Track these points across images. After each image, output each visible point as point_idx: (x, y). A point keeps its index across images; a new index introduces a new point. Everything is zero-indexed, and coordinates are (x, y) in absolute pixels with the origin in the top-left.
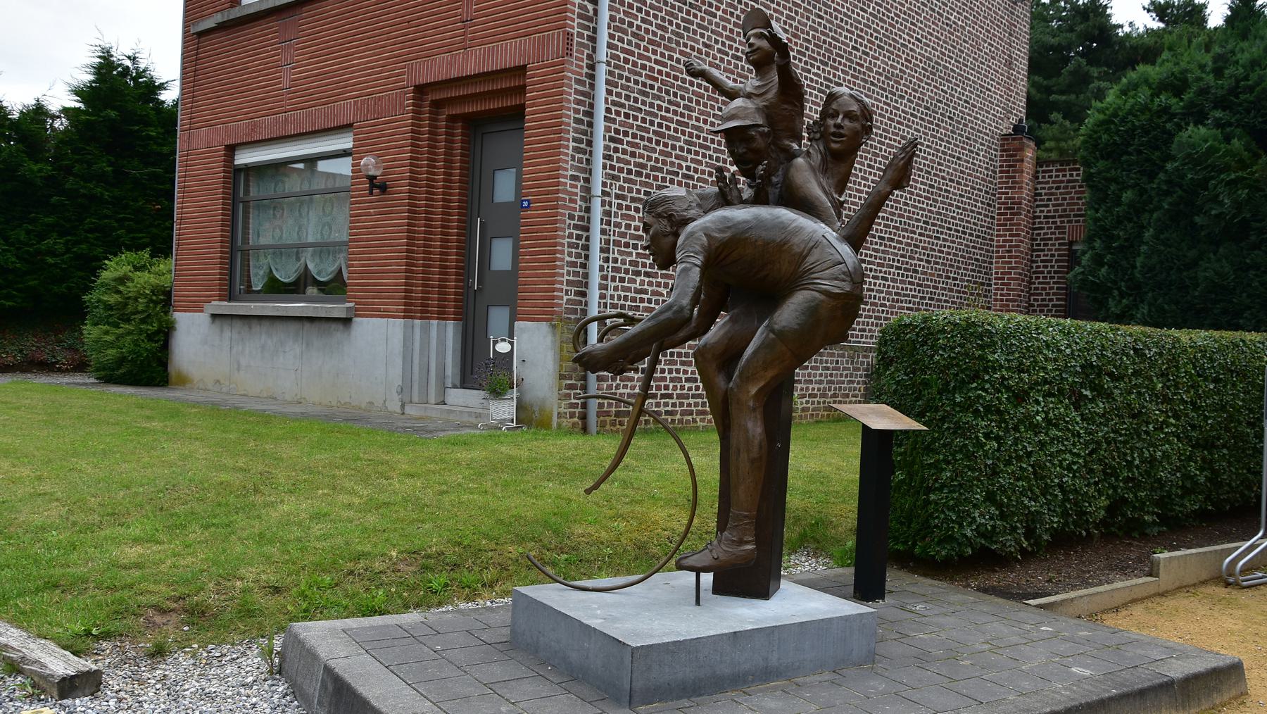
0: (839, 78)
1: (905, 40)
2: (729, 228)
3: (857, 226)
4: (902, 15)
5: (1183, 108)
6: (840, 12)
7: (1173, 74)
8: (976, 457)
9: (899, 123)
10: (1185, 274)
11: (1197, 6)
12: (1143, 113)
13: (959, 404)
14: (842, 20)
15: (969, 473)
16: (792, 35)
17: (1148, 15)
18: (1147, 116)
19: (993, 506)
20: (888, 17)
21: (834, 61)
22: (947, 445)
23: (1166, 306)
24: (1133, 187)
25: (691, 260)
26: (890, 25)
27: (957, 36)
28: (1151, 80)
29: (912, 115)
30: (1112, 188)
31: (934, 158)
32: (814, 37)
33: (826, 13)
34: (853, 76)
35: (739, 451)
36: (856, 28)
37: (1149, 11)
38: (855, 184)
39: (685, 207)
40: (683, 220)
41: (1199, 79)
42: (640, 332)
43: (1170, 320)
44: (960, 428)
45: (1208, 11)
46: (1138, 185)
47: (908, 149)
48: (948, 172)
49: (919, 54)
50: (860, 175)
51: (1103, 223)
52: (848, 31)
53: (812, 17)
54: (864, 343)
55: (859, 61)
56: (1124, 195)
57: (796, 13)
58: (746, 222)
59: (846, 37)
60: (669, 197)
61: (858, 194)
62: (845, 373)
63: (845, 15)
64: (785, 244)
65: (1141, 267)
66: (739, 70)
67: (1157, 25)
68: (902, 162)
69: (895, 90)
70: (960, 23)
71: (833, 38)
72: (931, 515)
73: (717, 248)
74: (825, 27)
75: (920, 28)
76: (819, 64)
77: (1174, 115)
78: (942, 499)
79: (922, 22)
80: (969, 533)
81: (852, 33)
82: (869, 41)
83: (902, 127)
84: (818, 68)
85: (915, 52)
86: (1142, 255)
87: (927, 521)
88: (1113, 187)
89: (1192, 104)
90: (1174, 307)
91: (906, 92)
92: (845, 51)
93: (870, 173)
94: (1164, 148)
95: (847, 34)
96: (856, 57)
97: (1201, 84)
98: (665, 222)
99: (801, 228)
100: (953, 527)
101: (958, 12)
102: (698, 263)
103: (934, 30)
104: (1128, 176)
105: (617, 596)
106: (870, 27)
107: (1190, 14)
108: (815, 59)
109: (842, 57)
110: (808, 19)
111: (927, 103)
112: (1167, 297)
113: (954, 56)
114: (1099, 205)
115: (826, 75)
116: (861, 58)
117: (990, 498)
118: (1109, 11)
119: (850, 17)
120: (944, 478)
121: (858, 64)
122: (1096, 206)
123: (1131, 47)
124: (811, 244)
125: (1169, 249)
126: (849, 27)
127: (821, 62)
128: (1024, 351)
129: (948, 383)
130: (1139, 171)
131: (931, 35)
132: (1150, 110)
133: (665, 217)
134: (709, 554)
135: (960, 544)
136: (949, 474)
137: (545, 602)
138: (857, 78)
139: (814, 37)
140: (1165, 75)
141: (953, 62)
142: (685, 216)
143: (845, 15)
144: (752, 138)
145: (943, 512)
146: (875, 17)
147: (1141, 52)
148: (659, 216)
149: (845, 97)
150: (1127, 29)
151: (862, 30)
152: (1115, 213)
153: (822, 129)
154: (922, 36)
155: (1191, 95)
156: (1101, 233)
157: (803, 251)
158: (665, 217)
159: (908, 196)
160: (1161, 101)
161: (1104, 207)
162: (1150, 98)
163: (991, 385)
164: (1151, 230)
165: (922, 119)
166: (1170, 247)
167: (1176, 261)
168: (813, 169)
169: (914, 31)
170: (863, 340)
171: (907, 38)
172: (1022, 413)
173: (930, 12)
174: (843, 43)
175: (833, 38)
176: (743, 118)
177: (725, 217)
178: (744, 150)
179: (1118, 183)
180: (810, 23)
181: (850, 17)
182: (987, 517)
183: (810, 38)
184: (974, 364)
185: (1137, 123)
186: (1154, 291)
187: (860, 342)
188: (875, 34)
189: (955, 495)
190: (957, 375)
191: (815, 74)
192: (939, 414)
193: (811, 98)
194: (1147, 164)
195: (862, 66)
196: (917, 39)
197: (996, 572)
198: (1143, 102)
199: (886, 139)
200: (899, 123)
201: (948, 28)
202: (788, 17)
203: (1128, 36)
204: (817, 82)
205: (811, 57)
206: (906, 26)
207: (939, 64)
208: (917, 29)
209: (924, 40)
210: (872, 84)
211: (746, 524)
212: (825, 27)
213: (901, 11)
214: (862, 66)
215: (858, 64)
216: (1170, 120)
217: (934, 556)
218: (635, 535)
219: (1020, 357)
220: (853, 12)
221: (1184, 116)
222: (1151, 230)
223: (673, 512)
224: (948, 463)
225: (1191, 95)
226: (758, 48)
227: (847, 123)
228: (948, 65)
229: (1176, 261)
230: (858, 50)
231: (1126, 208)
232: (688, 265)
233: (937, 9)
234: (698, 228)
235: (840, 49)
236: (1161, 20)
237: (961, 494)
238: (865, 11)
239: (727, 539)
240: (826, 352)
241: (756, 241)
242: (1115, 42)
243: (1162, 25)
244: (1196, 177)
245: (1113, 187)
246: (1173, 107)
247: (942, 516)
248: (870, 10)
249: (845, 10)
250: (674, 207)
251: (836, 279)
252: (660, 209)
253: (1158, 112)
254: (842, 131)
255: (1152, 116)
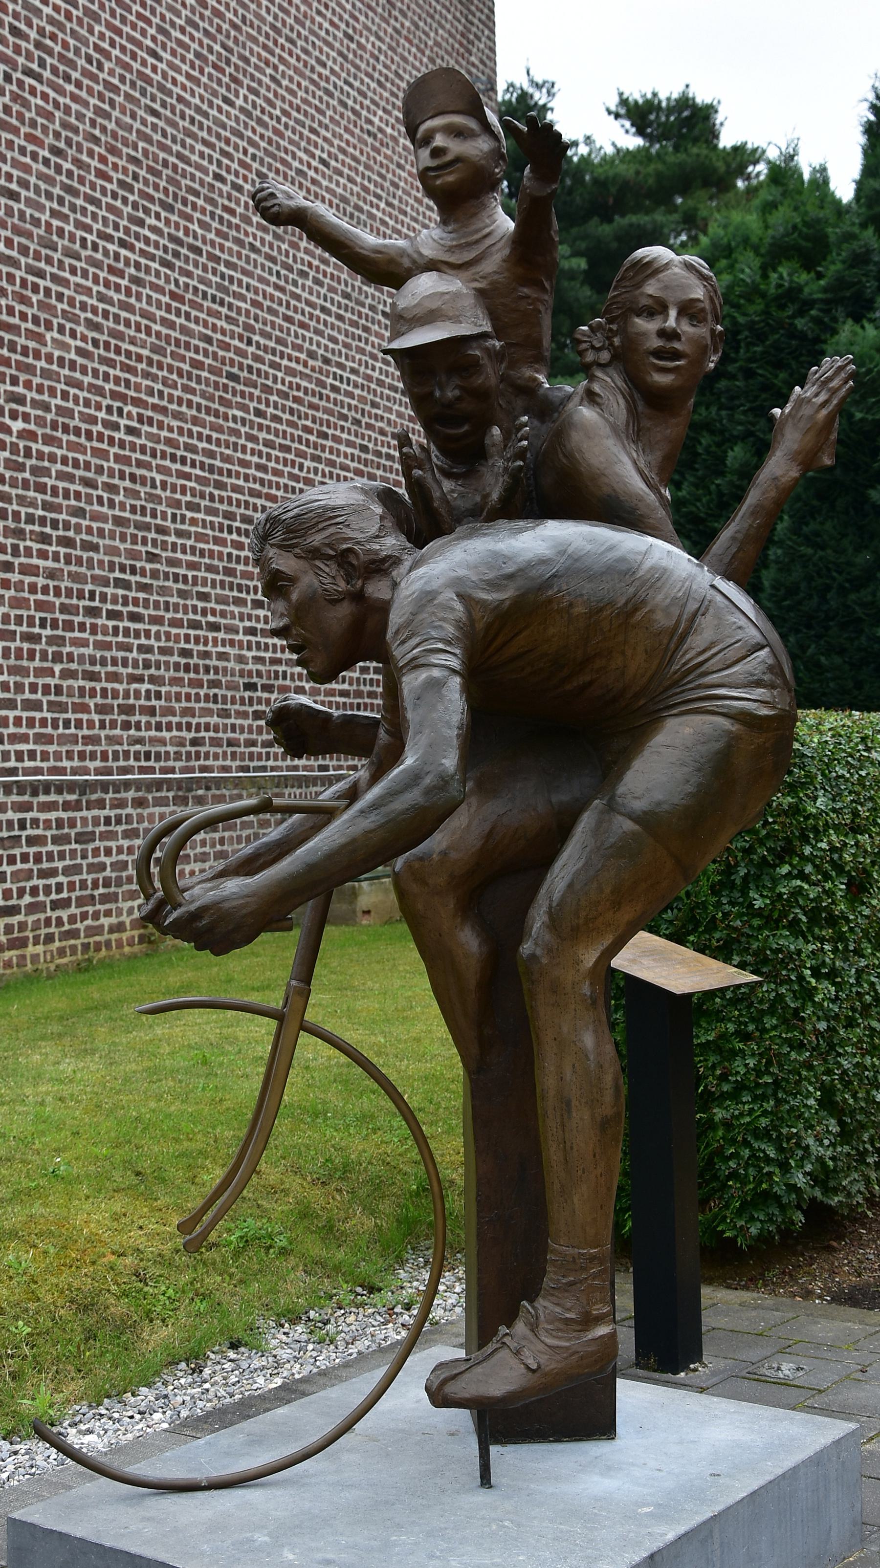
0: (195, 237)
1: (301, 161)
2: (511, 577)
3: (734, 557)
4: (294, 114)
5: (825, 290)
6: (188, 104)
7: (795, 227)
8: (803, 1019)
9: (303, 325)
10: (853, 597)
11: (701, 109)
12: (750, 301)
13: (759, 913)
14: (192, 121)
15: (793, 1055)
16: (107, 150)
17: (617, 124)
18: (759, 306)
19: (832, 1116)
20: (271, 116)
21: (185, 202)
22: (741, 1000)
23: (823, 659)
24: (744, 437)
25: (436, 659)
26: (276, 131)
27: (386, 157)
28: (754, 239)
29: (323, 309)
30: (703, 441)
31: (365, 394)
32: (146, 152)
33: (164, 105)
34: (218, 233)
35: (568, 1104)
36: (218, 136)
37: (617, 116)
38: (235, 450)
39: (373, 530)
40: (373, 562)
41: (849, 237)
42: (343, 846)
43: (832, 685)
44: (766, 961)
45: (719, 118)
46: (751, 434)
47: (835, 383)
48: (389, 420)
49: (328, 190)
50: (243, 430)
51: (694, 509)
52: (205, 142)
53: (141, 113)
54: (273, 769)
55: (226, 203)
56: (730, 454)
57: (112, 103)
58: (543, 562)
59: (202, 155)
60: (333, 509)
61: (242, 470)
62: (245, 833)
63: (198, 110)
64: (636, 609)
65: (773, 587)
66: (16, 220)
67: (633, 142)
68: (824, 412)
69: (290, 261)
70: (389, 130)
71: (179, 156)
72: (719, 1151)
73: (489, 627)
74: (164, 134)
75: (325, 139)
76: (158, 209)
77: (809, 304)
78: (742, 1115)
79: (327, 128)
80: (800, 1179)
81: (211, 146)
82: (242, 163)
83: (307, 334)
84: (158, 216)
85: (320, 185)
86: (773, 565)
87: (710, 1163)
88: (706, 440)
89: (840, 284)
90: (838, 660)
91: (310, 265)
92: (202, 183)
93: (260, 427)
94: (794, 365)
95: (203, 148)
96: (221, 195)
97: (855, 245)
98: (330, 568)
99: (665, 570)
100: (770, 1174)
101: (385, 110)
102: (455, 663)
103: (348, 143)
104: (731, 418)
105: (278, 1492)
106: (241, 136)
107: (689, 122)
108: (151, 199)
109: (197, 194)
110: (133, 116)
111: (346, 285)
112: (822, 642)
113: (384, 195)
114: (682, 475)
115: (173, 231)
116: (229, 197)
117: (828, 1103)
118: (549, 116)
119: (206, 115)
120: (742, 1070)
121: (226, 209)
122: (676, 477)
123: (595, 181)
124: (692, 606)
125: (821, 553)
126: (205, 134)
127: (162, 204)
128: (857, 788)
129: (729, 870)
130: (751, 409)
131: (344, 152)
132: (763, 295)
133: (330, 557)
134: (514, 1362)
135: (783, 1208)
136: (751, 1062)
137: (133, 1550)
138: (225, 237)
139: (146, 152)
140: (781, 229)
141: (382, 205)
142: (376, 552)
143: (198, 110)
144: (474, 365)
145: (746, 1143)
146: (249, 115)
147: (613, 190)
148: (314, 554)
149: (676, 270)
150: (583, 150)
151: (227, 142)
152: (713, 487)
153: (617, 341)
154: (330, 154)
155: (839, 266)
156: (689, 526)
157: (678, 622)
158: (330, 557)
159: (327, 470)
160: (781, 277)
161: (692, 479)
162: (760, 272)
163: (815, 866)
164: (786, 517)
165: (340, 318)
166: (823, 548)
167: (835, 574)
168: (614, 428)
169: (316, 146)
170: (271, 763)
171: (305, 157)
172: (867, 917)
173: (340, 109)
174: (199, 167)
175: (179, 156)
176: (456, 319)
177: (496, 555)
178: (457, 392)
179: (712, 432)
180: (137, 125)
181: (206, 115)
182: (826, 1142)
183: (139, 156)
184: (783, 824)
185: (741, 320)
186: (797, 631)
187: (264, 769)
188: (251, 150)
189: (770, 1105)
190: (747, 851)
191: (153, 229)
192: (717, 935)
193: (148, 278)
194: (764, 396)
195: (232, 212)
196: (323, 162)
197: (834, 1250)
198: (748, 280)
199: (282, 357)
200: (303, 325)
201: (370, 140)
202: (98, 111)
203: (585, 160)
204: (157, 245)
205: (143, 195)
206: (301, 135)
207: (361, 210)
208: (320, 141)
209: (333, 163)
210: (253, 248)
211: (594, 1276)
212: (164, 134)
213: (291, 104)
214: (232, 212)
215: (226, 209)
216: (801, 313)
217: (733, 1240)
218: (64, 1278)
219: (852, 801)
220: (211, 104)
221: (829, 305)
222: (786, 517)
223: (117, 1207)
224: (746, 1037)
225: (839, 266)
226: (458, 160)
227: (686, 328)
228: (374, 211)
229: (835, 574)
230: (222, 180)
231: (735, 478)
232: (436, 673)
233: (350, 103)
234: (441, 581)
235: (193, 178)
236: (640, 132)
237: (779, 1102)
238: (231, 104)
239: (553, 1319)
240: (210, 793)
241: (571, 605)
242: (567, 173)
243: (639, 142)
244: (870, 417)
245: (706, 440)
246: (806, 290)
247: (746, 1153)
248: (240, 102)
249: (197, 101)
250: (349, 533)
251: (758, 684)
252: (316, 539)
253: (778, 298)
254: (677, 345)
255: (767, 306)
